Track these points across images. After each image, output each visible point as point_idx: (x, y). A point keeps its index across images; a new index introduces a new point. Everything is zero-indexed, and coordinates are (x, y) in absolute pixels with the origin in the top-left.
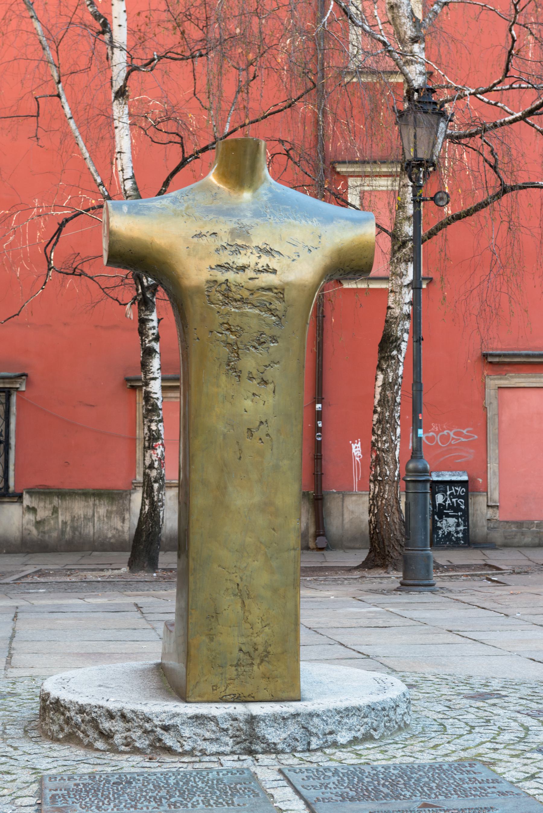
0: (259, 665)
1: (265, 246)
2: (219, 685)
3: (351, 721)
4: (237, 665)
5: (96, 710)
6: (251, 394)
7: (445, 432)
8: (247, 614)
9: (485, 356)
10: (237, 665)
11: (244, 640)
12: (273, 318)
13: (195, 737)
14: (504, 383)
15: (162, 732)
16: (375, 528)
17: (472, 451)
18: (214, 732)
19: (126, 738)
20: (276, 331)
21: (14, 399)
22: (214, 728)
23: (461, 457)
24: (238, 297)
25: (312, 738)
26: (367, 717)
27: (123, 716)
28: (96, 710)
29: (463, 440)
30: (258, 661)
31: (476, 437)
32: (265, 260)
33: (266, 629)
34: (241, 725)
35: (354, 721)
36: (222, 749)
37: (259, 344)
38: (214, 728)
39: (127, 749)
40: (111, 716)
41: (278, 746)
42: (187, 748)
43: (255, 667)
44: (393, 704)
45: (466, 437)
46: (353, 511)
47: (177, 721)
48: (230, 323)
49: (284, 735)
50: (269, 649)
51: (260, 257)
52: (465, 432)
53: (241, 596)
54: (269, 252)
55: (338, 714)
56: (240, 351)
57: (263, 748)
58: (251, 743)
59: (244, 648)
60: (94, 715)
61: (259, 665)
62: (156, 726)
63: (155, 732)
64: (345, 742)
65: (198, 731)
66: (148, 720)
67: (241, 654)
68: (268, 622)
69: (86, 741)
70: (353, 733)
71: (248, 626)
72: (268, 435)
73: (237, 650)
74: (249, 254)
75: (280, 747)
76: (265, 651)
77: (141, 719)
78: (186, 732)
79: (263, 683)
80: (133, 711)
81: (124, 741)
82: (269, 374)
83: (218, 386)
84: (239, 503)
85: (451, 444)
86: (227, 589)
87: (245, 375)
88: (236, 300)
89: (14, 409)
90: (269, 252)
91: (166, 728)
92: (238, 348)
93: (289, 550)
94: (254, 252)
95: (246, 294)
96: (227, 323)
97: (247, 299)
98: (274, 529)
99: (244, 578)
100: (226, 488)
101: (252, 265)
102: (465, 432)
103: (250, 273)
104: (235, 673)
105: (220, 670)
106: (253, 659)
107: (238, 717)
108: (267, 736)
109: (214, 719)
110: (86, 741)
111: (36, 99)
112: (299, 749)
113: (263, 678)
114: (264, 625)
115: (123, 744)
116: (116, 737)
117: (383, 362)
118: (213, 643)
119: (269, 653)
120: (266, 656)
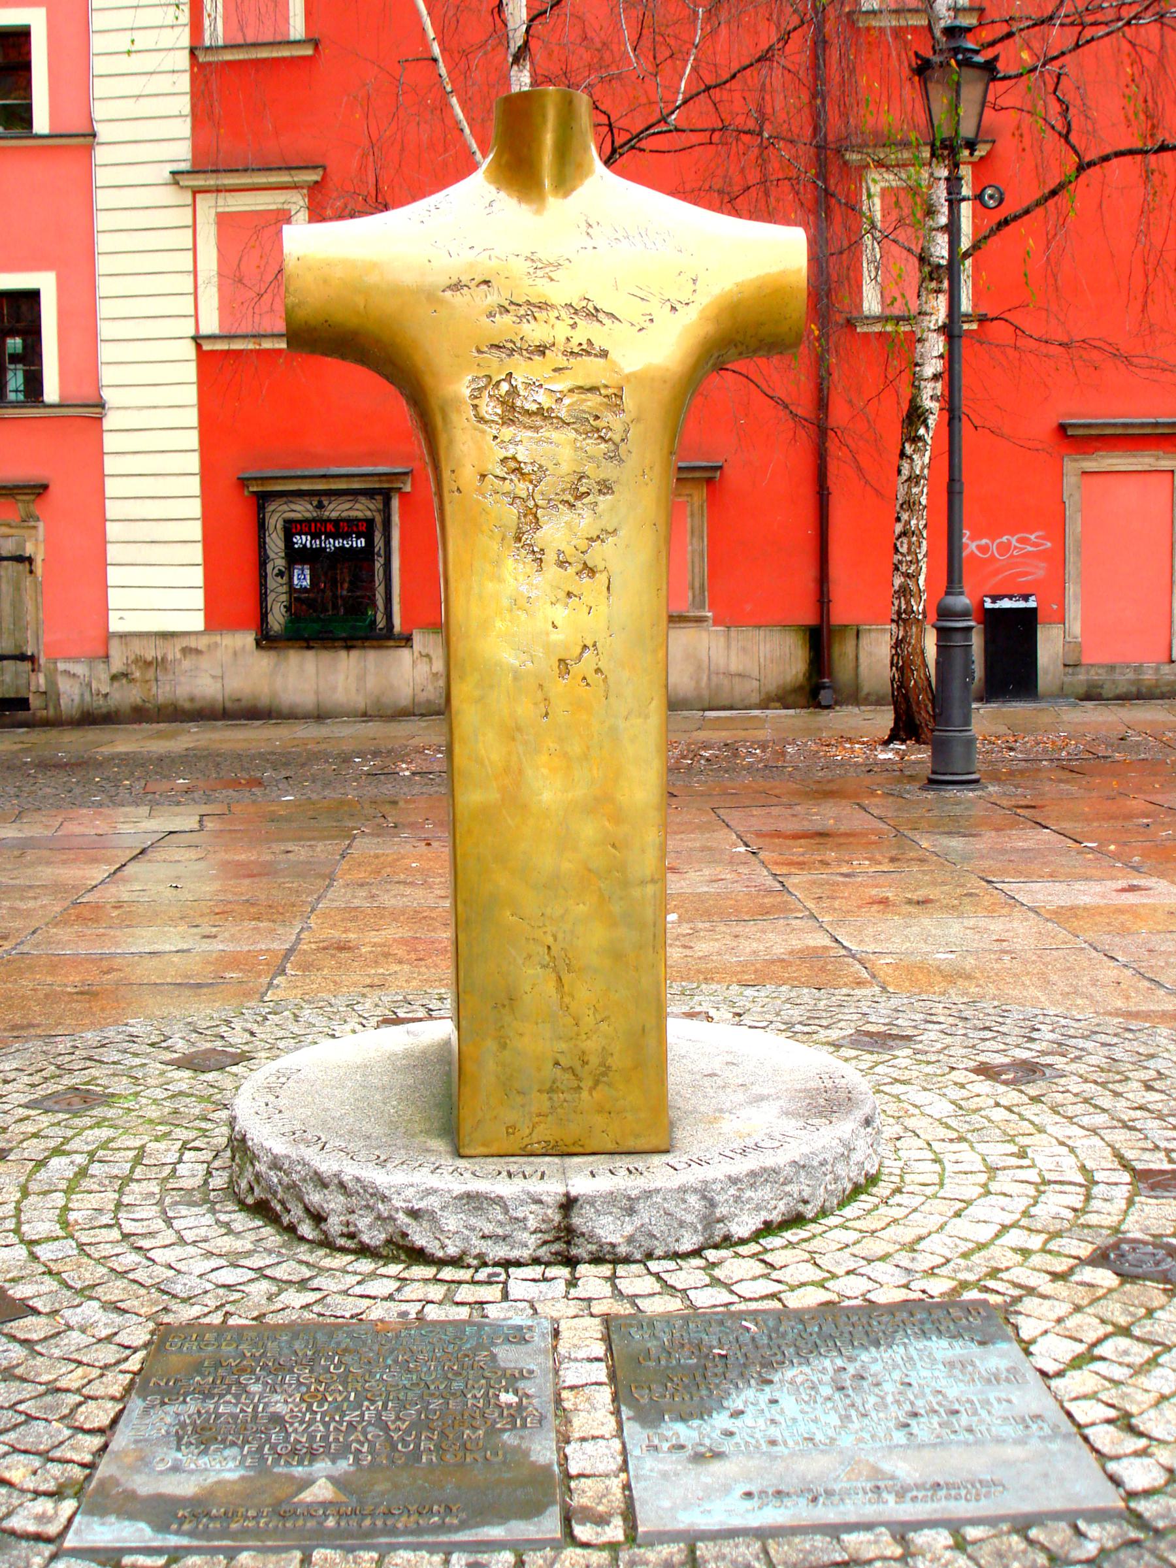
0: (591, 1089)
1: (584, 303)
2: (518, 1126)
3: (760, 1193)
4: (552, 1090)
5: (299, 1168)
6: (562, 595)
7: (1004, 539)
8: (567, 1000)
9: (1062, 428)
10: (552, 1090)
11: (563, 1046)
12: (603, 446)
13: (467, 1232)
14: (1090, 465)
15: (407, 1220)
16: (899, 688)
17: (1043, 565)
18: (501, 1224)
19: (348, 1224)
20: (609, 471)
21: (395, 503)
22: (500, 1217)
23: (1026, 574)
24: (534, 407)
25: (683, 1232)
26: (791, 1182)
27: (342, 1185)
28: (299, 1168)
29: (1030, 549)
30: (590, 1083)
31: (1049, 545)
32: (586, 331)
33: (604, 1026)
34: (549, 1211)
35: (764, 1193)
36: (515, 1254)
37: (578, 498)
38: (500, 1217)
39: (350, 1244)
40: (321, 1182)
41: (619, 1250)
42: (452, 1251)
43: (585, 1094)
44: (841, 1150)
45: (1035, 545)
46: (872, 655)
47: (432, 1202)
48: (520, 458)
49: (629, 1229)
50: (610, 1061)
51: (574, 326)
52: (1032, 537)
53: (555, 968)
54: (594, 314)
55: (735, 1183)
56: (540, 512)
57: (591, 1253)
58: (568, 1243)
59: (564, 1061)
60: (295, 1177)
61: (591, 1089)
62: (397, 1210)
63: (395, 1220)
64: (746, 1235)
65: (473, 1221)
66: (384, 1199)
67: (558, 1071)
68: (606, 1014)
69: (286, 1220)
70: (764, 1215)
71: (569, 1020)
72: (598, 670)
73: (550, 1065)
74: (553, 320)
75: (623, 1250)
76: (603, 1064)
77: (372, 1195)
78: (451, 1222)
79: (599, 1120)
80: (358, 1180)
81: (345, 1230)
82: (598, 555)
83: (501, 580)
84: (547, 796)
85: (1012, 556)
86: (530, 956)
87: (550, 557)
88: (528, 413)
89: (396, 519)
90: (594, 314)
91: (414, 1214)
92: (537, 506)
93: (643, 883)
94: (564, 314)
95: (546, 401)
96: (514, 458)
97: (550, 409)
98: (614, 846)
99: (560, 936)
100: (521, 772)
101: (561, 340)
102: (1032, 537)
103: (555, 358)
104: (548, 1104)
105: (519, 1100)
106: (580, 1080)
107: (544, 1198)
108: (598, 1231)
109: (499, 1201)
110: (286, 1220)
111: (1081, 168)
112: (659, 1252)
113: (599, 1112)
114: (599, 1017)
115: (342, 1235)
116: (330, 1220)
117: (907, 445)
118: (506, 1053)
119: (609, 1068)
120: (604, 1074)
